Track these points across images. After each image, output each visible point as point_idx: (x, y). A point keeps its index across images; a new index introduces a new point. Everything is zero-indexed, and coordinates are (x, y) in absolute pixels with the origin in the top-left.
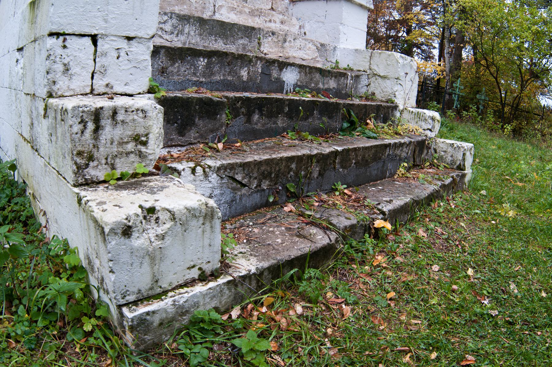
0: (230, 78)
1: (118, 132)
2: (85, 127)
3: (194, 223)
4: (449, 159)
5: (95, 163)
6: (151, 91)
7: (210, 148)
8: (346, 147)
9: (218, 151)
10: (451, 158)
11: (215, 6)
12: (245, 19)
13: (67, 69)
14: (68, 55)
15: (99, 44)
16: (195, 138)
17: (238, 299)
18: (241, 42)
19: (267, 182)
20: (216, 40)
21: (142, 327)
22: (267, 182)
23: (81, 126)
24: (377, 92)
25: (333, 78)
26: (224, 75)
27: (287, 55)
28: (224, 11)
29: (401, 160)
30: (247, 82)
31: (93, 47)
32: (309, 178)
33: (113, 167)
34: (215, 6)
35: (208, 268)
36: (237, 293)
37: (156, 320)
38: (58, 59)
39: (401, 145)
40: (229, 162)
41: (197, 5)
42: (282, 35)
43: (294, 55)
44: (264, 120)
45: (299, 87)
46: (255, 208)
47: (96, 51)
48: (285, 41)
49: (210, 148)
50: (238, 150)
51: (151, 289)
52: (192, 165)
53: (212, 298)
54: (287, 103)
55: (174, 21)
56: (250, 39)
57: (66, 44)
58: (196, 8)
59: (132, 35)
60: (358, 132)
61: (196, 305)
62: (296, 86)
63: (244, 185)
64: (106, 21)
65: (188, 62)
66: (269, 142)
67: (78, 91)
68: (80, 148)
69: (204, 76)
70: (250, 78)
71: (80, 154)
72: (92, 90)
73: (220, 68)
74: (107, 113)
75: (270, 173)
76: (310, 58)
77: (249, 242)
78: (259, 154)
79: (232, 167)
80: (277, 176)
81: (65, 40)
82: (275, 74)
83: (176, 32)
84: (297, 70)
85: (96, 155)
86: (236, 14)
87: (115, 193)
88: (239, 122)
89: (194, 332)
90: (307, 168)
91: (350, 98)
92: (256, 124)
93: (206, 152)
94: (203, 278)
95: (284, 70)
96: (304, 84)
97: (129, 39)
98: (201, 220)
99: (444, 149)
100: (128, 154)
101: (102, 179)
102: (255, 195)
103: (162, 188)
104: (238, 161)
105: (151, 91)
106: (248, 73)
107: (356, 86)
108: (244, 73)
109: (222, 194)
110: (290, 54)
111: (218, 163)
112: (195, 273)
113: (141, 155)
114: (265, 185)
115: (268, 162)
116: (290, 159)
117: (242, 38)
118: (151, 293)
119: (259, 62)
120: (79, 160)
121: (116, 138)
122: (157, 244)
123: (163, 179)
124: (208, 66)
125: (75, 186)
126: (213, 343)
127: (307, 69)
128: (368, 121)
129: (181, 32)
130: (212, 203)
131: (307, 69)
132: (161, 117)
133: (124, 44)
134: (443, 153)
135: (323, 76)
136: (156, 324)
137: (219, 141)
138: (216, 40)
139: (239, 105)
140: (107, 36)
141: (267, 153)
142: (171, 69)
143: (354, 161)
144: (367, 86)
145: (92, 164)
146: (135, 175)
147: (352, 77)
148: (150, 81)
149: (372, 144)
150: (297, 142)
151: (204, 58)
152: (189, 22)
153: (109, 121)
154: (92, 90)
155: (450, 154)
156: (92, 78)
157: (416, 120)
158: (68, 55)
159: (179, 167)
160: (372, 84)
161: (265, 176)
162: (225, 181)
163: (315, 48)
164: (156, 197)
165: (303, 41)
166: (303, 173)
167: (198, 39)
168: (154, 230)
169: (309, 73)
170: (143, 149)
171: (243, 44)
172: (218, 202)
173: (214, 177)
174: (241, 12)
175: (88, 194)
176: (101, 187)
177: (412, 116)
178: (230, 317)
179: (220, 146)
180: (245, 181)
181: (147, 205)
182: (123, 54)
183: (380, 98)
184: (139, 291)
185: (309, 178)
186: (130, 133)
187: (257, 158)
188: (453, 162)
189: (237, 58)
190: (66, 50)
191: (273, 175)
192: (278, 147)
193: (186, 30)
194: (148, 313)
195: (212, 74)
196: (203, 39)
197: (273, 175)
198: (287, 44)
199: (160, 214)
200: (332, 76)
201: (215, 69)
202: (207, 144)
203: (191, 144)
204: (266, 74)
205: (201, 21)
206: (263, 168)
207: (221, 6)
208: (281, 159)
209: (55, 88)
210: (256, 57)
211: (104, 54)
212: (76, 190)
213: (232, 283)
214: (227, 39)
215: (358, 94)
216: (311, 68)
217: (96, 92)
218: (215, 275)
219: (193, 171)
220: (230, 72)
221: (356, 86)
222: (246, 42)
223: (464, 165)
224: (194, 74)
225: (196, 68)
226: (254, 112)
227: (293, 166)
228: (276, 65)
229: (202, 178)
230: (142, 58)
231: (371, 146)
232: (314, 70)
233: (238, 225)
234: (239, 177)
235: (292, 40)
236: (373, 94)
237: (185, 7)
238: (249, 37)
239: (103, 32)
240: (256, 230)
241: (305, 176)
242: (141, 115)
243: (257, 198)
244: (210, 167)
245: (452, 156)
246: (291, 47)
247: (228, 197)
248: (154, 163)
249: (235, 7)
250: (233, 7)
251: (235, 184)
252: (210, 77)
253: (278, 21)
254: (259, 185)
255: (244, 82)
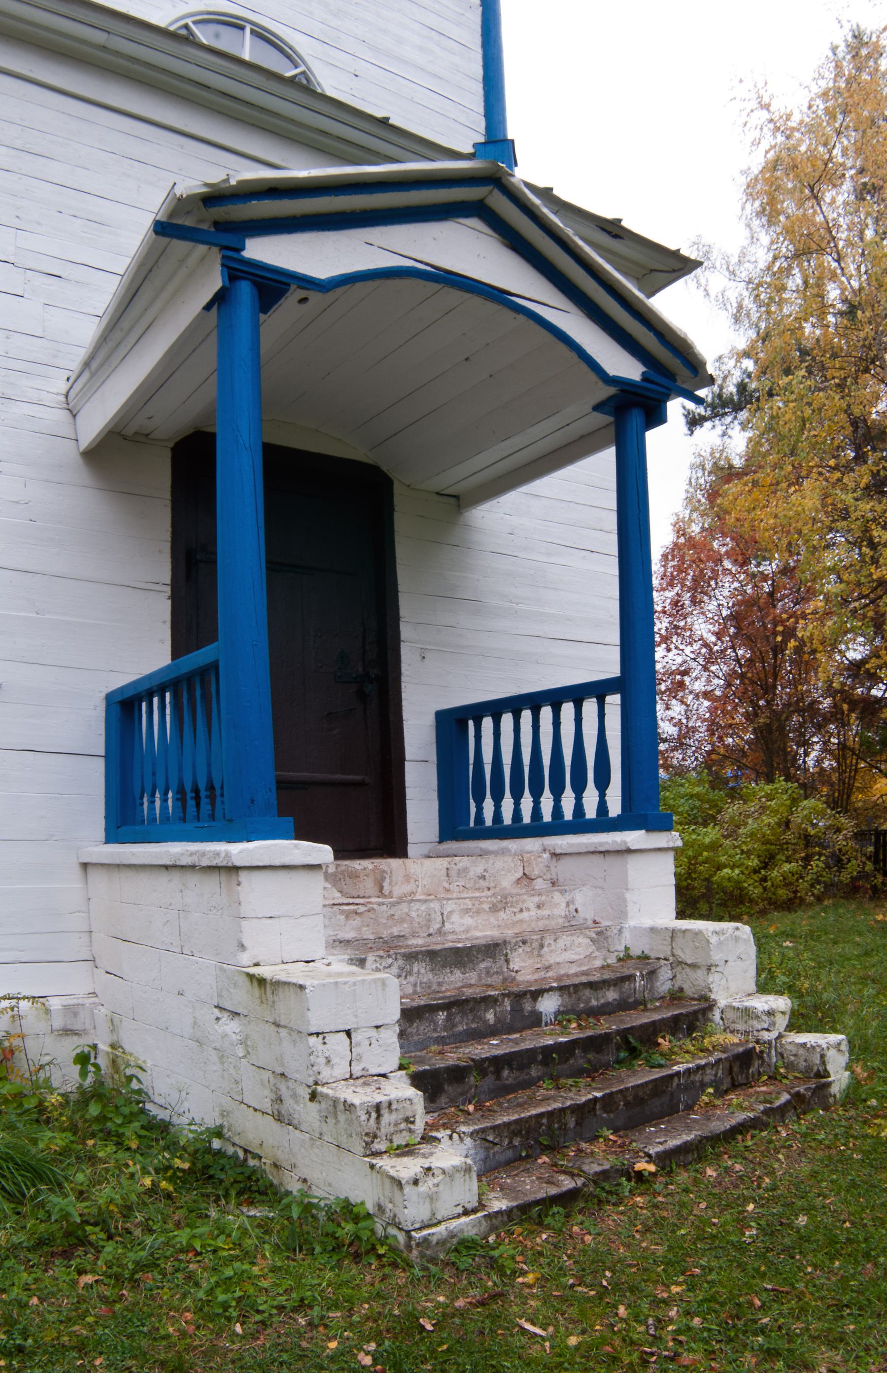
0: (474, 1026)
1: (394, 1117)
2: (370, 1116)
3: (458, 1175)
4: (802, 1064)
5: (379, 1140)
6: (401, 1067)
7: (461, 1111)
8: (607, 1091)
9: (469, 1114)
10: (804, 1064)
11: (442, 914)
12: (486, 920)
13: (328, 1061)
14: (328, 1050)
15: (353, 1036)
16: (446, 1103)
17: (493, 1229)
18: (483, 965)
19: (519, 1139)
20: (451, 972)
21: (425, 1245)
22: (519, 1139)
23: (367, 1116)
24: (686, 987)
25: (612, 988)
26: (467, 1024)
27: (547, 964)
28: (455, 918)
29: (703, 1086)
30: (495, 1025)
31: (348, 1040)
32: (564, 1129)
33: (391, 1141)
34: (442, 914)
35: (469, 1206)
36: (492, 1225)
37: (434, 1240)
38: (320, 1054)
39: (699, 1068)
40: (481, 1126)
41: (420, 920)
42: (537, 940)
43: (558, 960)
44: (516, 1073)
45: (562, 1017)
46: (508, 1163)
47: (351, 1043)
48: (542, 946)
49: (461, 1111)
50: (490, 1110)
51: (430, 1219)
52: (449, 1132)
53: (473, 1227)
54: (540, 1050)
55: (401, 962)
56: (494, 959)
57: (326, 1040)
58: (419, 923)
59: (380, 1024)
60: (642, 1060)
61: (462, 1231)
62: (558, 1013)
63: (496, 1144)
64: (356, 1016)
65: (427, 1019)
66: (522, 1096)
67: (340, 1077)
68: (367, 1131)
69: (445, 1030)
70: (498, 1020)
71: (367, 1134)
72: (351, 1075)
73: (462, 1017)
74: (385, 1105)
75: (520, 1131)
76: (582, 957)
77: (502, 1189)
78: (508, 1115)
79: (483, 1130)
80: (528, 1132)
81: (324, 1038)
82: (527, 1006)
83: (404, 974)
84: (557, 993)
85: (379, 1134)
86: (471, 917)
87: (396, 1159)
88: (489, 1081)
89: (461, 1248)
90: (560, 1121)
91: (642, 1007)
92: (507, 1079)
93: (459, 1116)
94: (466, 1213)
95: (540, 999)
96: (569, 1007)
97: (377, 1027)
98: (463, 1173)
99: (794, 1052)
100: (401, 1131)
101: (384, 1150)
102: (507, 1152)
103: (431, 1154)
104: (489, 1125)
105: (401, 1067)
106: (495, 1015)
107: (651, 987)
108: (490, 1016)
109: (476, 1154)
110: (552, 962)
111: (471, 1129)
112: (460, 1210)
113: (410, 1131)
114: (516, 1142)
115: (516, 1122)
116: (541, 1115)
117: (484, 960)
118: (430, 1222)
119: (506, 999)
120: (366, 1139)
121: (393, 1121)
122: (435, 1189)
123: (429, 1146)
124: (449, 1019)
125: (364, 1156)
126: (475, 1255)
127: (571, 989)
128: (660, 1040)
129: (410, 973)
130: (469, 1161)
131: (571, 989)
132: (422, 1100)
133: (373, 1033)
134: (792, 1058)
135: (596, 990)
136: (434, 1242)
137: (470, 1103)
138: (451, 972)
139: (486, 1065)
140: (358, 1028)
141: (516, 1112)
142: (409, 1030)
143: (622, 1103)
144: (672, 979)
145: (376, 1141)
146: (407, 1145)
147: (642, 976)
148: (400, 1059)
149: (647, 1079)
150: (552, 1092)
151: (443, 1012)
152: (417, 960)
153: (387, 1110)
154: (351, 1075)
155: (802, 1058)
156: (350, 1065)
157: (744, 1019)
158: (328, 1050)
159: (439, 1135)
160: (679, 976)
161: (515, 1134)
162: (478, 1142)
163: (589, 940)
164: (430, 1160)
165: (569, 938)
166: (556, 1125)
167: (431, 976)
168: (431, 1181)
169: (575, 993)
170: (412, 1126)
171: (486, 968)
172: (474, 1160)
173: (468, 1141)
174: (478, 912)
175: (378, 1162)
176: (385, 1156)
177: (739, 1014)
178: (487, 1242)
179: (471, 1108)
180: (496, 1141)
181: (426, 1166)
182: (374, 1041)
183: (692, 995)
184: (422, 1221)
185: (564, 1129)
186: (402, 1117)
187: (506, 1119)
188: (809, 1068)
189: (480, 1002)
190: (326, 1046)
191: (524, 1132)
192: (532, 1101)
193: (415, 969)
194: (429, 1235)
195: (454, 1025)
196: (436, 974)
197: (524, 1132)
198: (546, 949)
199: (435, 1171)
200: (609, 986)
201: (457, 1020)
202: (458, 1107)
203: (443, 1109)
204: (517, 1010)
205: (432, 955)
206: (513, 1127)
207: (451, 912)
208: (530, 1117)
209: (320, 1077)
210: (503, 994)
211: (358, 1044)
212: (367, 1159)
213: (488, 1217)
214: (465, 967)
215: (656, 995)
216: (576, 986)
217: (354, 1077)
218: (474, 1211)
219: (451, 1137)
220: (473, 1019)
221: (651, 987)
222: (489, 965)
223: (826, 1070)
224: (435, 1030)
225: (436, 1024)
226: (503, 1068)
227: (544, 1121)
228: (528, 996)
229: (458, 1142)
230: (391, 1041)
231: (646, 1083)
232: (581, 987)
233: (492, 1177)
234: (490, 1138)
235: (552, 942)
236: (681, 990)
237: (405, 925)
238: (493, 957)
239: (355, 1026)
240: (508, 1181)
241: (560, 1128)
242: (408, 1102)
243: (510, 1154)
244: (464, 1133)
245: (806, 1061)
246: (551, 951)
247: (482, 1154)
248: (420, 1136)
249: (470, 907)
250: (467, 909)
251: (487, 1144)
252: (451, 1029)
253: (532, 906)
254: (510, 1142)
255: (490, 1026)
